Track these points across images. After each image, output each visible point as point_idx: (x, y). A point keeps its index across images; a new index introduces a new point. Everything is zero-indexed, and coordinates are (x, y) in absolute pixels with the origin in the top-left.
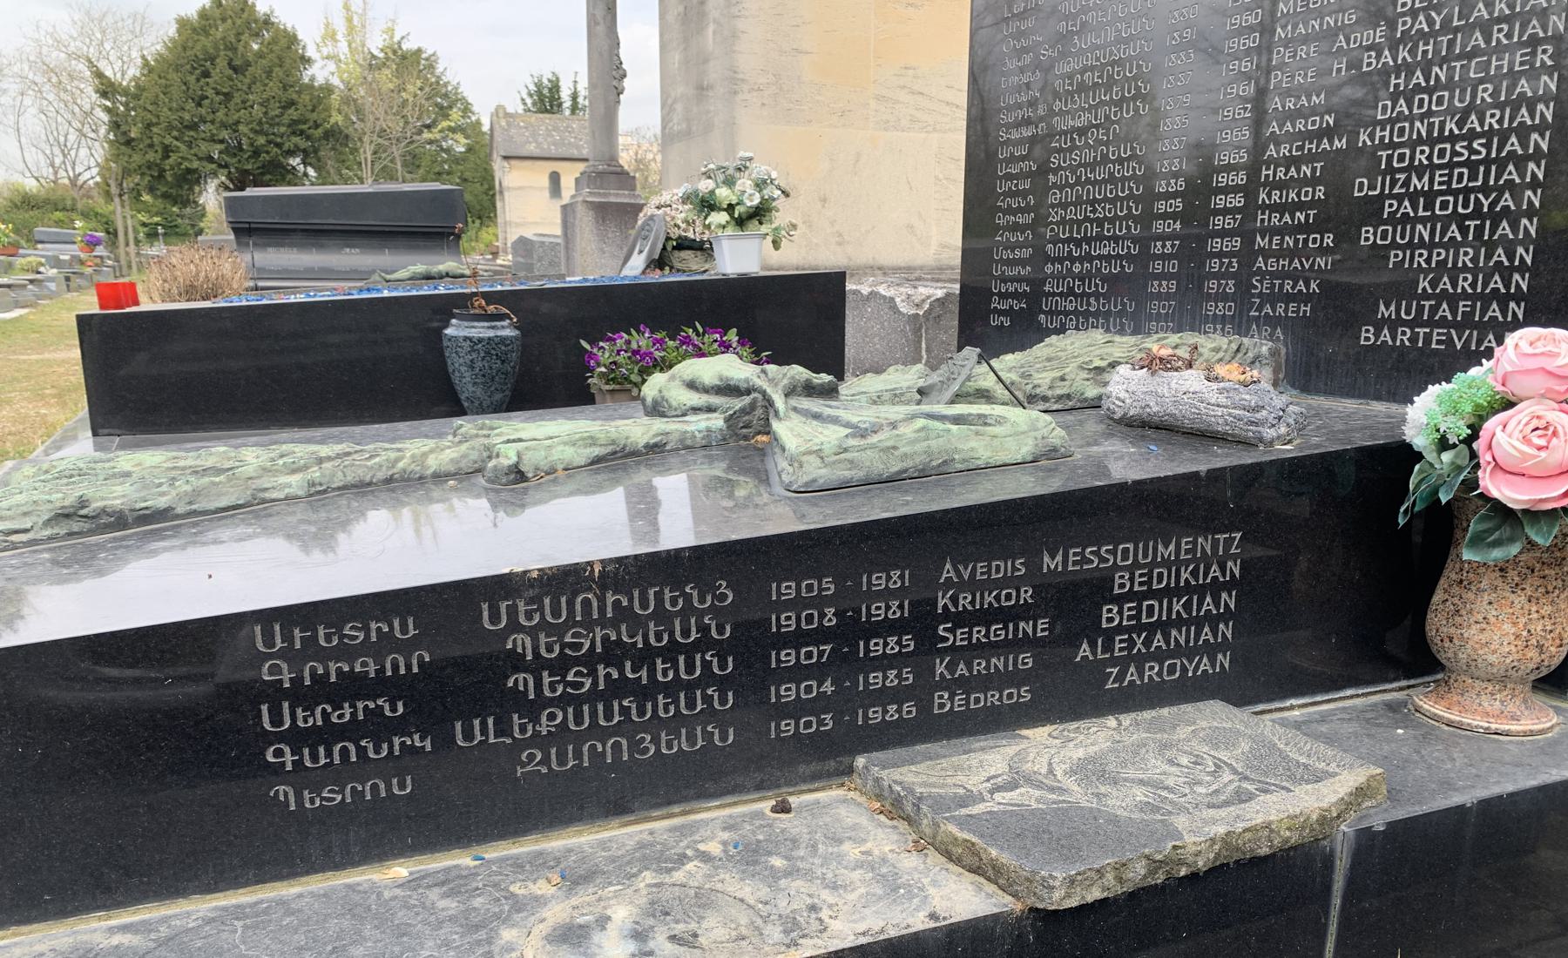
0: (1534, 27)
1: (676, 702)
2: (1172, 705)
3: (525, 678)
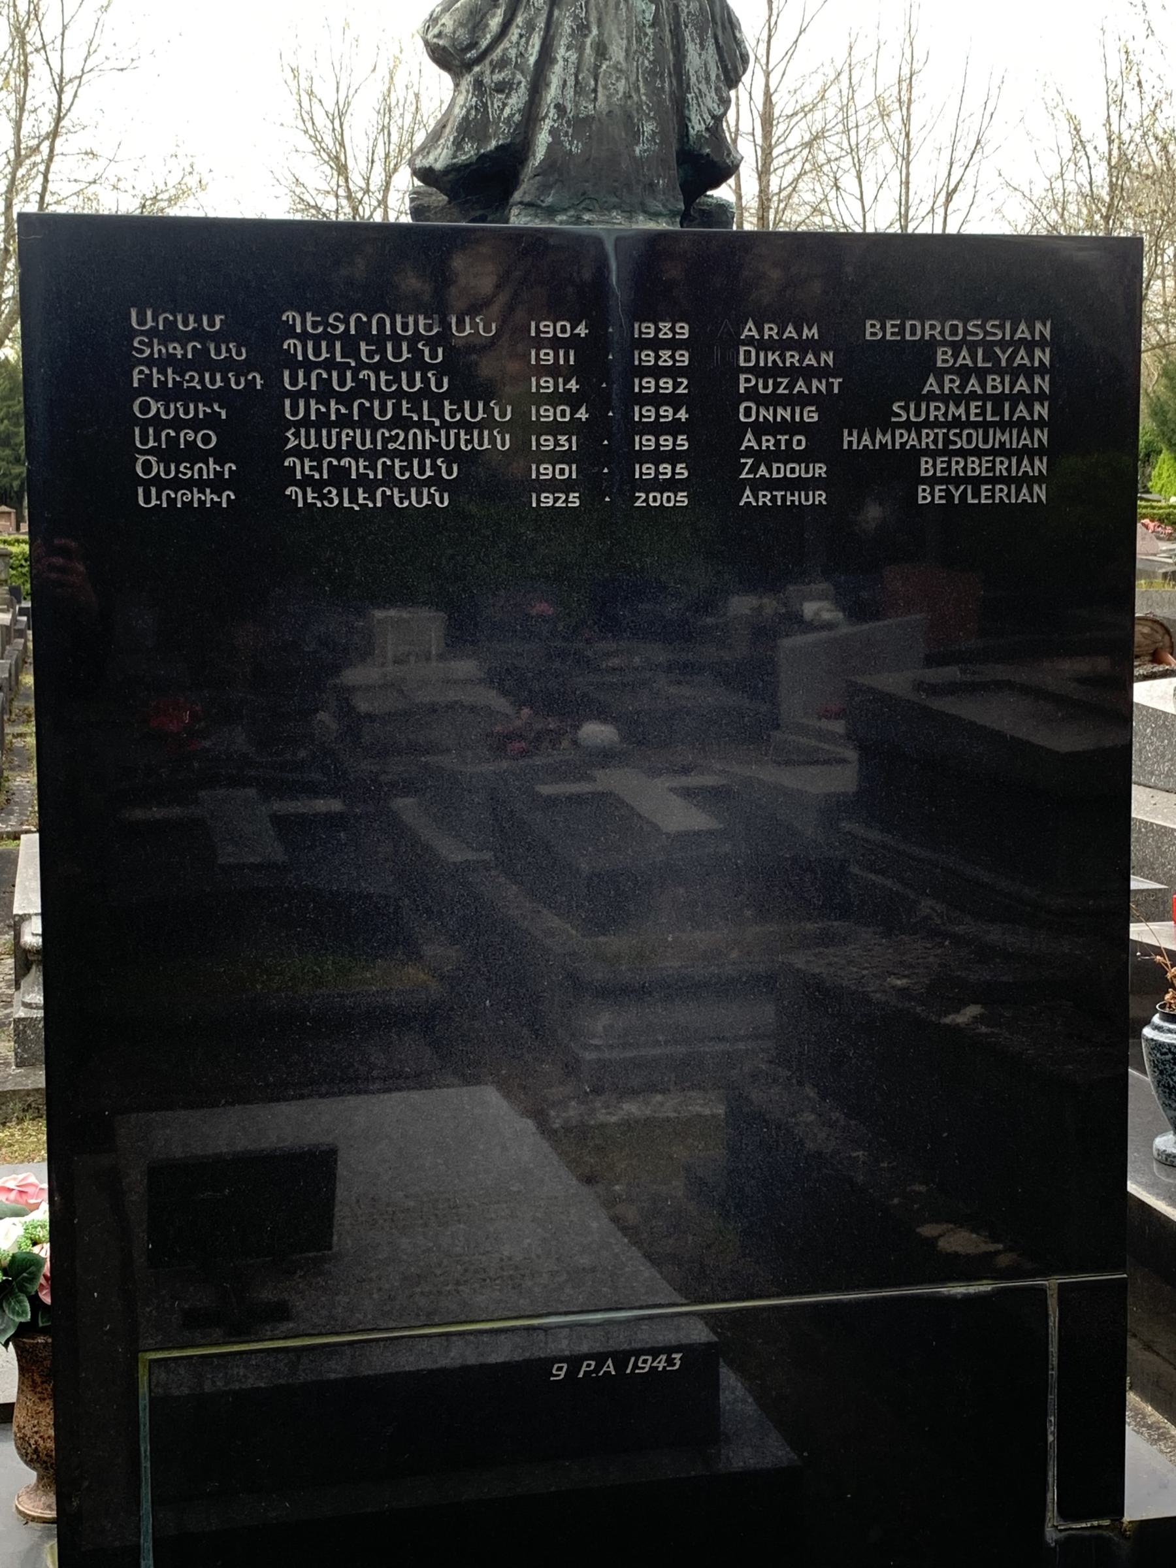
0: (749, 441)
1: (461, 409)
2: (443, 1371)
3: (294, 316)
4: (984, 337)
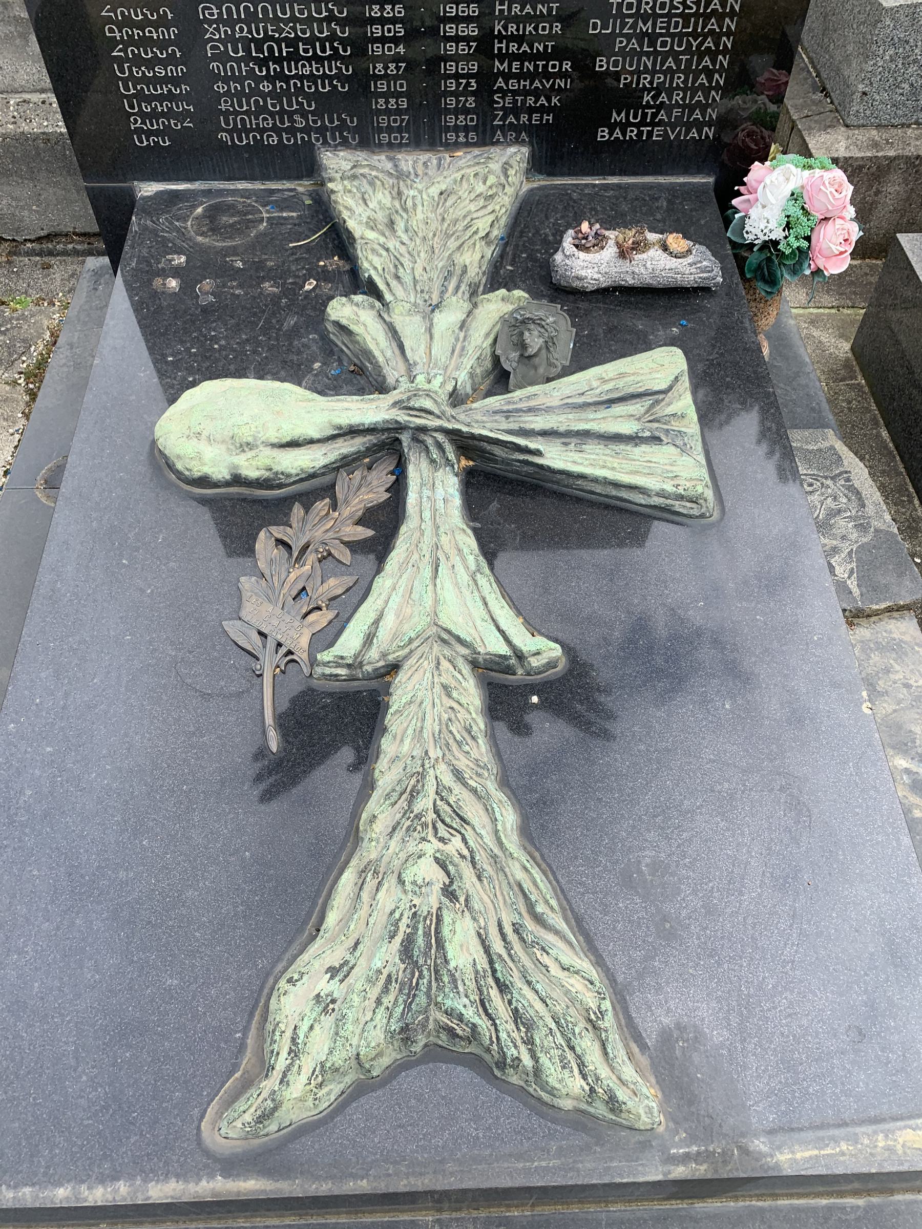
4: (684, 10)
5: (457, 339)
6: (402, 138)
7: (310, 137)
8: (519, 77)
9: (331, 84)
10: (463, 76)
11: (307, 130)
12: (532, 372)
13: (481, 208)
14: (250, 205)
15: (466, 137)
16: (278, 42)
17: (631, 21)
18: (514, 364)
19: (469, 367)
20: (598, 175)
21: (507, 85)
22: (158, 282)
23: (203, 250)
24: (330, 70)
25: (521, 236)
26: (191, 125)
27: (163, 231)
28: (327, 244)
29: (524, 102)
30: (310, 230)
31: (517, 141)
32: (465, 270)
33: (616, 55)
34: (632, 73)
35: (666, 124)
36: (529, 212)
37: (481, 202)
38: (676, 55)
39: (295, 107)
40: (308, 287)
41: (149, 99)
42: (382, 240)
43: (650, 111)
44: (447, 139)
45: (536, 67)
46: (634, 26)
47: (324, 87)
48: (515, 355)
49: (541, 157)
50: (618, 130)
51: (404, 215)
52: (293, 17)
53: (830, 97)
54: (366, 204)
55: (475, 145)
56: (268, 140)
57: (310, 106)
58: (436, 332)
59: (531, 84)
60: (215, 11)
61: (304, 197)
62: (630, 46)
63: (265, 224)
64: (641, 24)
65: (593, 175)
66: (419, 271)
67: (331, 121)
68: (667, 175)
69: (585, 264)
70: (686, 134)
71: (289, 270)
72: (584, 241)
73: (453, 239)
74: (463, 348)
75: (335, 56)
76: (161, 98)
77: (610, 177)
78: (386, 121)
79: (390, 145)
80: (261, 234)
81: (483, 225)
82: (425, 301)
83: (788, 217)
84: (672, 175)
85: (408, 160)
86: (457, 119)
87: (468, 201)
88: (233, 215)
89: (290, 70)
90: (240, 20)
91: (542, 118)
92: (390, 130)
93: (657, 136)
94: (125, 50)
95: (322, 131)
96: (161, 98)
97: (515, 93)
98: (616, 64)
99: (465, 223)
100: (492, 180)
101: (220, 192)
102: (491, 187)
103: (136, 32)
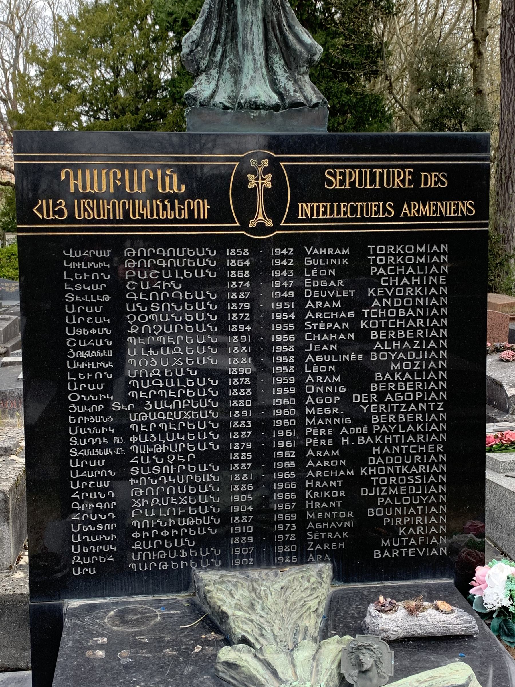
5: (313, 666)
6: (249, 561)
7: (189, 563)
8: (322, 521)
9: (206, 530)
10: (288, 522)
11: (188, 559)
12: (369, 683)
13: (310, 595)
14: (146, 608)
15: (290, 559)
16: (176, 507)
17: (385, 488)
18: (355, 679)
19: (325, 680)
20: (377, 581)
21: (315, 526)
22: (89, 653)
23: (118, 634)
24: (207, 521)
25: (336, 615)
26: (113, 559)
27: (88, 625)
28: (204, 627)
29: (326, 536)
30: (191, 619)
31: (323, 560)
32: (306, 629)
33: (379, 507)
34: (390, 517)
35: (415, 547)
36: (338, 603)
37: (309, 592)
38: (415, 506)
39: (182, 545)
40: (196, 650)
41: (88, 545)
42: (247, 616)
43: (404, 539)
44: (278, 561)
45: (332, 515)
46: (387, 491)
47: (201, 532)
48: (355, 672)
49: (339, 570)
50: (386, 551)
51: (260, 601)
52: (187, 493)
53: (508, 556)
54: (233, 597)
55: (296, 564)
56: (161, 567)
57: (191, 544)
58: (298, 662)
59: (329, 525)
60: (141, 492)
61: (184, 603)
62: (387, 502)
63: (159, 618)
64: (391, 490)
65: (374, 581)
66: (276, 631)
67: (204, 553)
68: (423, 579)
69: (387, 621)
70: (430, 553)
71: (181, 641)
72: (383, 608)
73: (294, 613)
74: (318, 671)
75: (211, 513)
76: (96, 544)
77: (385, 582)
78: (239, 551)
79: (241, 566)
80: (157, 623)
81: (313, 604)
82: (285, 646)
83: (510, 591)
84: (426, 579)
85: (254, 574)
86: (284, 548)
87: (300, 591)
88: (136, 614)
89: (181, 523)
90: (155, 496)
91: (338, 545)
92: (241, 556)
93: (412, 554)
94: (80, 516)
95: (197, 559)
96: (96, 544)
97: (320, 531)
98: (380, 512)
99: (301, 603)
100: (313, 580)
101: (125, 603)
102: (313, 584)
103: (90, 505)
